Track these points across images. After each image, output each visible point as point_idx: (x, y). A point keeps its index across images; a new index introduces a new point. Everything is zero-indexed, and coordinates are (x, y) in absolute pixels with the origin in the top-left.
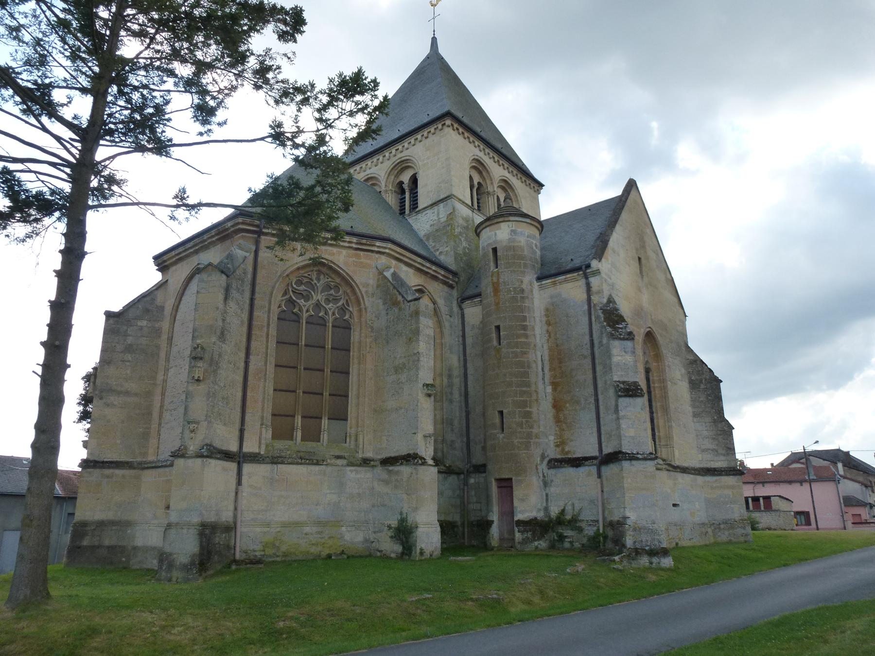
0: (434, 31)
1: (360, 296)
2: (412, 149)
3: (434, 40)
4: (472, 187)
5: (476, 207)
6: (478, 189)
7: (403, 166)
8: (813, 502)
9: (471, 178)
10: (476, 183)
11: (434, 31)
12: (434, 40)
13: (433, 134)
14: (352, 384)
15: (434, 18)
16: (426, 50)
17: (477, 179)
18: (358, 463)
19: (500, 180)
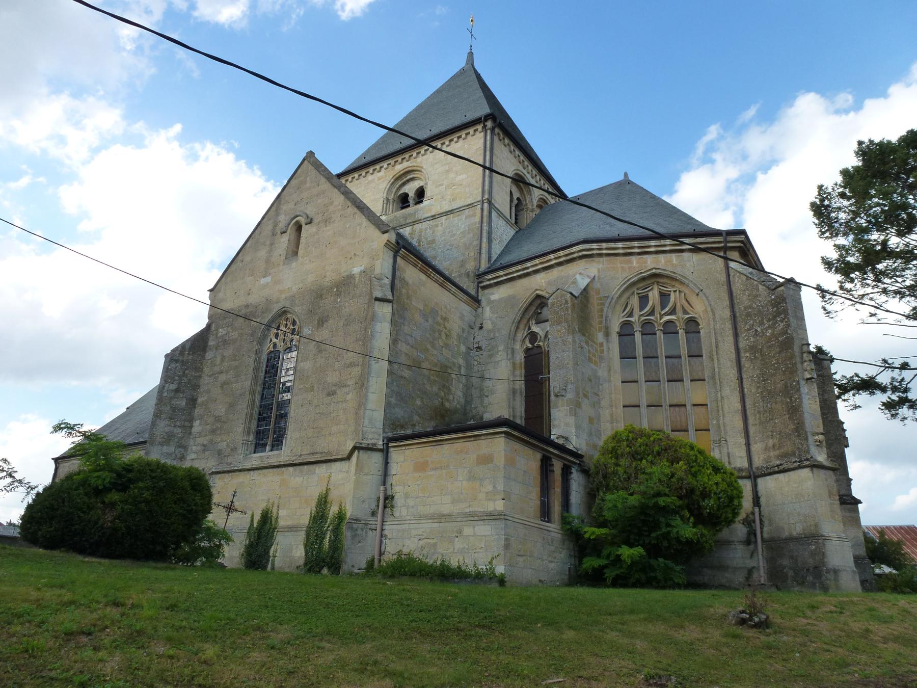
0: (471, 46)
1: (637, 278)
2: (419, 159)
3: (471, 55)
4: (511, 201)
5: (513, 221)
6: (517, 206)
7: (405, 177)
8: (854, 362)
9: (511, 193)
10: (515, 197)
11: (471, 46)
12: (471, 55)
13: (364, 177)
14: (404, 445)
15: (472, 35)
16: (462, 63)
17: (516, 195)
18: (494, 562)
19: (541, 198)
